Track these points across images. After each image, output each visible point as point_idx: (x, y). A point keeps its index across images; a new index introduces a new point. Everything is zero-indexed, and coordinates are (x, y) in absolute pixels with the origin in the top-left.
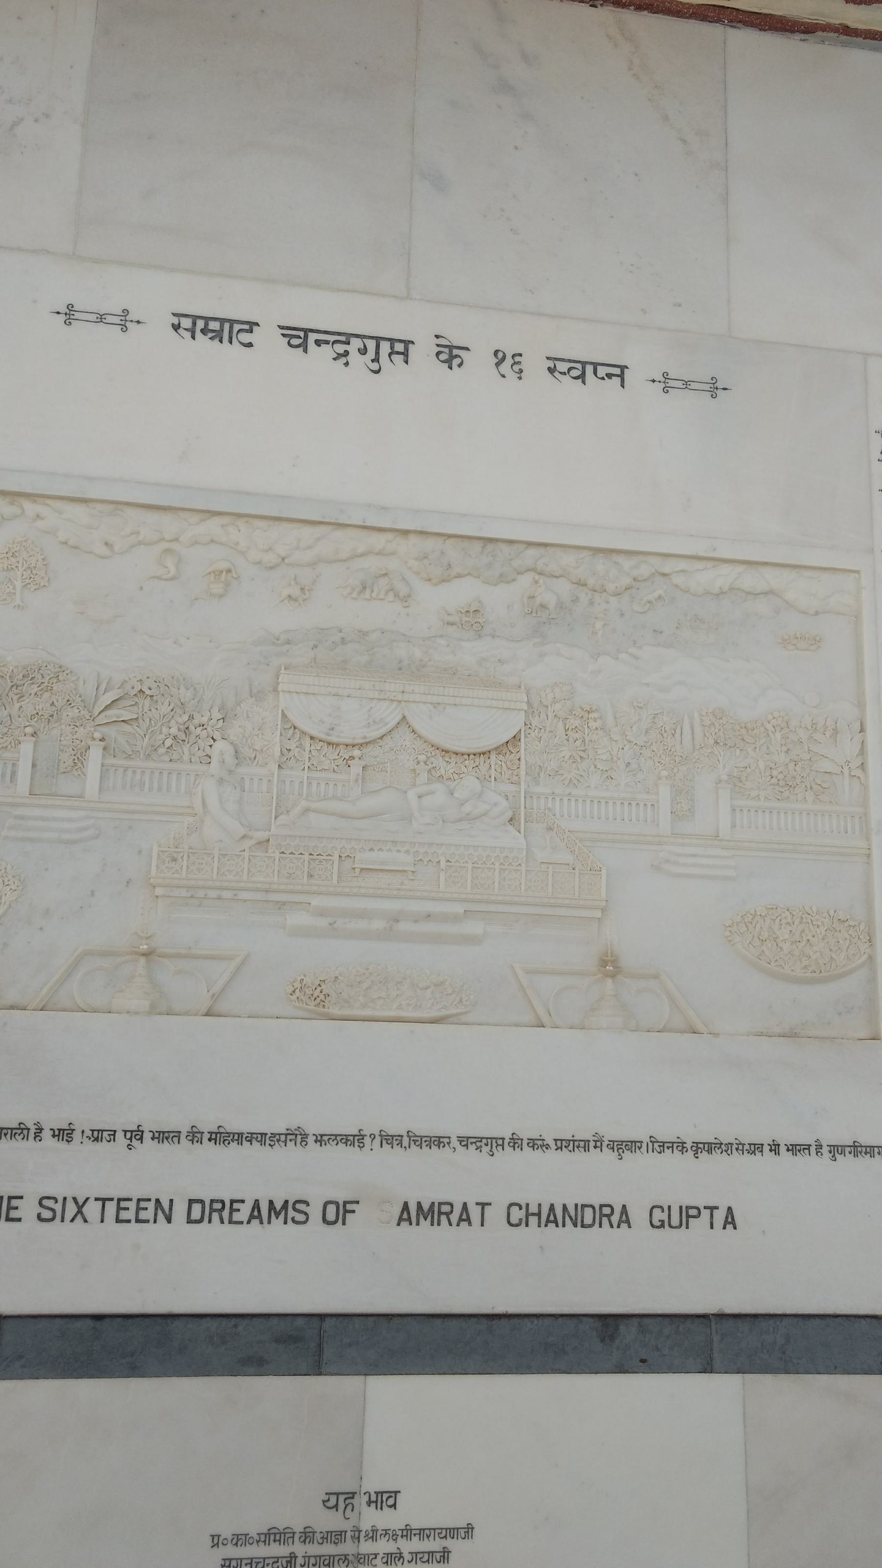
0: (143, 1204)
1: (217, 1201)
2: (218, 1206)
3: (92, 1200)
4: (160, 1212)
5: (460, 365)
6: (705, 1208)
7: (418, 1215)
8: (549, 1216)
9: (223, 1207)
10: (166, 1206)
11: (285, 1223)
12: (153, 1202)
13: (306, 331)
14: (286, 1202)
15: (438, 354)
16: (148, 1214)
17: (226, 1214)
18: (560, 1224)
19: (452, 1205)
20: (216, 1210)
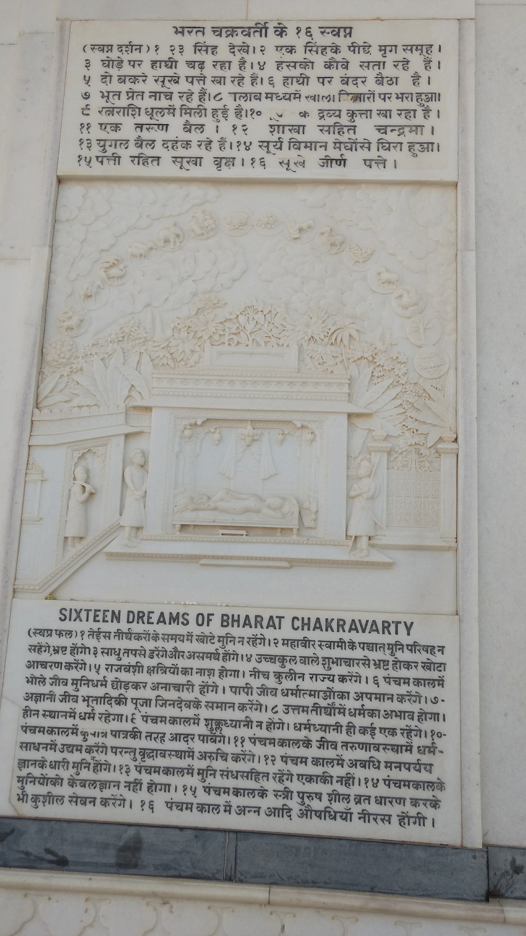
0: (98, 613)
1: (341, 620)
2: (141, 615)
3: (83, 611)
4: (364, 626)
5: (286, 35)
6: (277, 617)
7: (170, 620)
8: (315, 624)
9: (228, 619)
10: (117, 613)
11: (178, 624)
12: (110, 612)
13: (386, 126)
14: (178, 613)
15: (275, 31)
16: (109, 618)
17: (145, 619)
18: (277, 627)
19: (262, 619)
20: (386, 627)
